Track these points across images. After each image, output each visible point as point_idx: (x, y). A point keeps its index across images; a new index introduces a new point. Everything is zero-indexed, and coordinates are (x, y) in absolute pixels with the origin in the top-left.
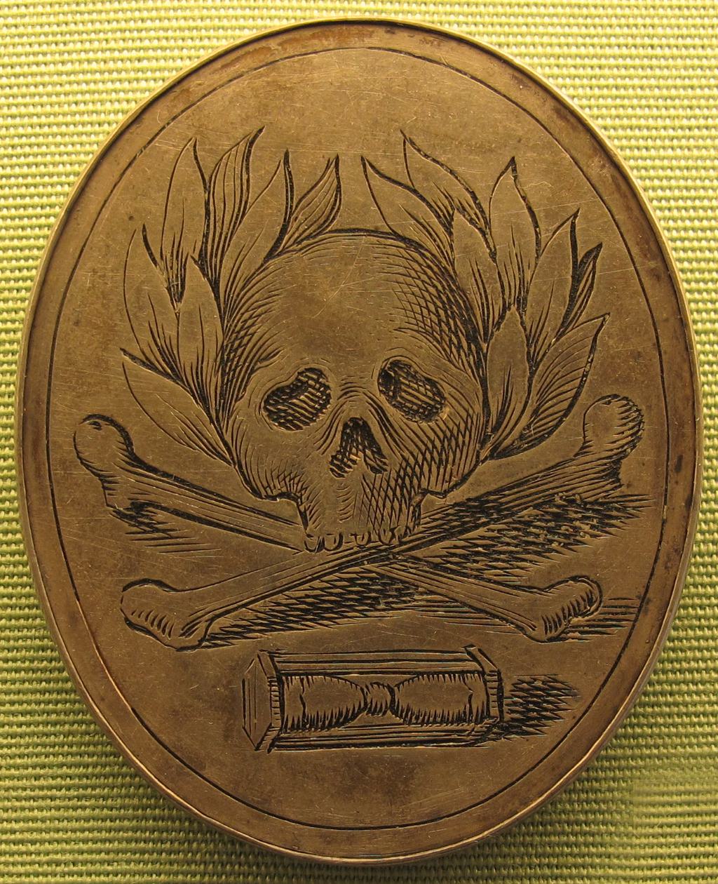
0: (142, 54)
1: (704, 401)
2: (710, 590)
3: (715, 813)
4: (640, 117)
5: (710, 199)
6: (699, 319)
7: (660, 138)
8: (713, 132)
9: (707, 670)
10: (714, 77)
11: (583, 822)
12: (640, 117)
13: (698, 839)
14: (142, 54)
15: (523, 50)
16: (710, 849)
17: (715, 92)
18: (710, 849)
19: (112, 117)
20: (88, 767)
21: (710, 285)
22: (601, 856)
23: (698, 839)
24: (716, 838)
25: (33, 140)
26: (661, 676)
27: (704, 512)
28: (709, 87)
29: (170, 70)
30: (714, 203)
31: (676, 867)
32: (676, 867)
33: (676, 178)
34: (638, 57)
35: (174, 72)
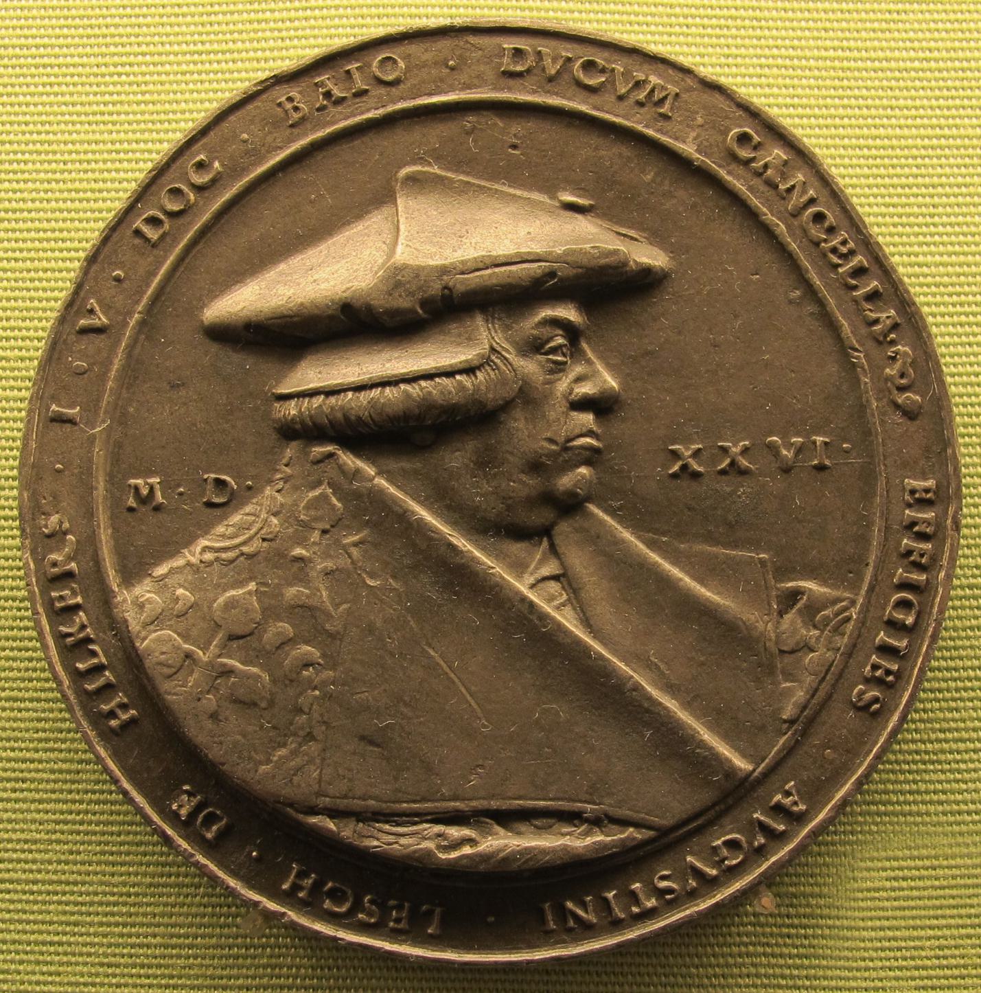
0: (333, 31)
1: (964, 481)
2: (974, 735)
3: (977, 886)
4: (867, 138)
5: (973, 235)
12: (867, 138)
13: (883, 954)
14: (333, 31)
17: (979, 673)
19: (158, 146)
21: (974, 121)
23: (883, 954)
24: (979, 981)
25: (19, 176)
26: (746, 960)
27: (961, 568)
33: (921, 98)
34: (781, 967)
35: (352, 38)
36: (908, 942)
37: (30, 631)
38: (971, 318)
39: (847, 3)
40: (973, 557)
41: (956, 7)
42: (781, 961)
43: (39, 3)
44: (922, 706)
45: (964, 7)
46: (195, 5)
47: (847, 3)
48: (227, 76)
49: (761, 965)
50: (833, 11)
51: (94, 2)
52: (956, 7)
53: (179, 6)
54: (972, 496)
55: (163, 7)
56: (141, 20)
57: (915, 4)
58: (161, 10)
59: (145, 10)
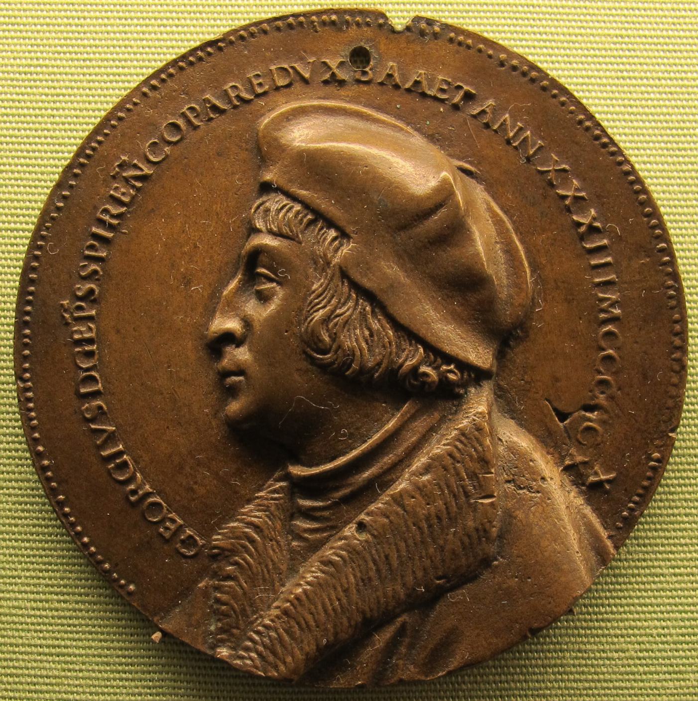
2: (693, 481)
6: (683, 266)
7: (649, 71)
8: (695, 153)
9: (691, 471)
10: (695, 58)
11: (588, 605)
15: (532, 50)
16: (693, 593)
18: (693, 593)
20: (180, 674)
22: (13, 691)
28: (692, 38)
29: (147, 68)
30: (696, 231)
31: (66, 647)
32: (66, 647)
36: (672, 675)
37: (11, 385)
38: (691, 117)
39: (584, 2)
40: (692, 418)
41: (640, 5)
42: (644, 564)
43: (246, 2)
44: (676, 468)
45: (646, 5)
46: (421, 4)
47: (584, 2)
48: (25, 154)
49: (641, 538)
50: (120, 47)
51: (198, 2)
52: (640, 5)
53: (73, 4)
54: (691, 280)
55: (404, 4)
56: (109, 28)
57: (611, 3)
58: (402, 7)
59: (478, 7)
